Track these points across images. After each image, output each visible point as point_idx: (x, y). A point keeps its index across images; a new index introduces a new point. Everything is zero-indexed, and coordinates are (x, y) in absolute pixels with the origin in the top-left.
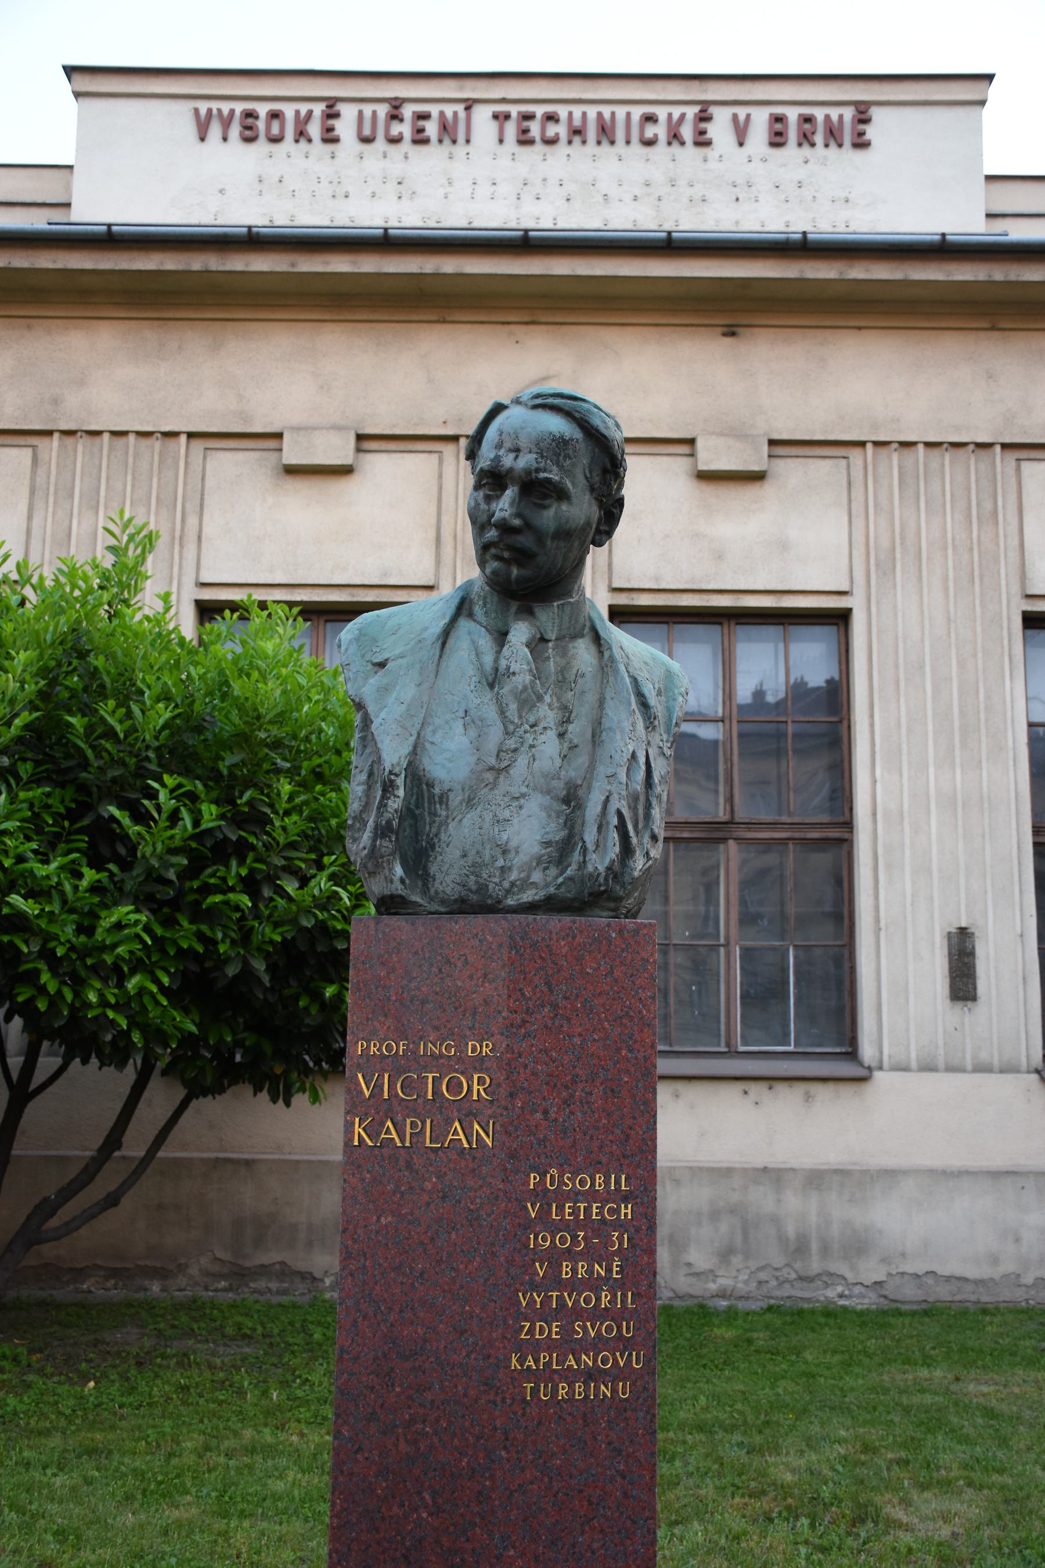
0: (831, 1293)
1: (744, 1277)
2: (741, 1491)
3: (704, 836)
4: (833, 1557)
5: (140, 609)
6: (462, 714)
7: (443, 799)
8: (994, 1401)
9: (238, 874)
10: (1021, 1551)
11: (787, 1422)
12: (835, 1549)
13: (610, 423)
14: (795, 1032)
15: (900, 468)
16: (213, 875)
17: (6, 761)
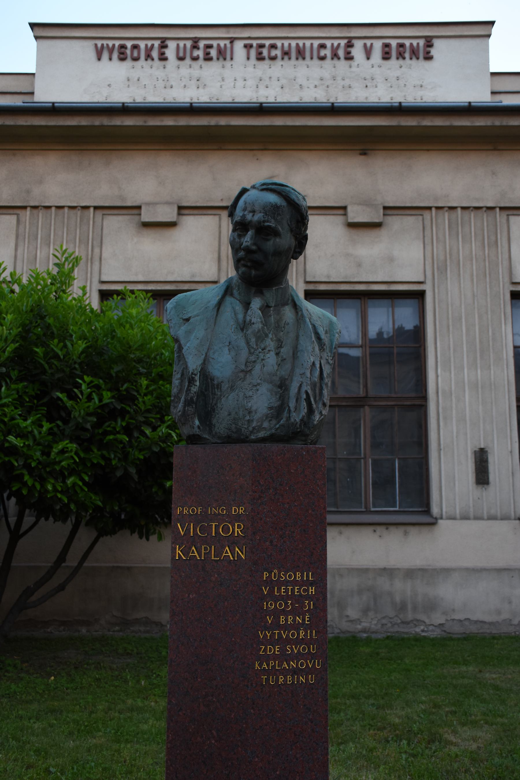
0: (418, 630)
1: (375, 622)
2: (373, 728)
4: (419, 759)
5: (71, 294)
6: (227, 344)
7: (219, 386)
8: (499, 682)
9: (121, 425)
10: (511, 755)
11: (396, 693)
12: (420, 755)
13: (300, 197)
14: (399, 501)
15: (449, 220)
16: (109, 426)
17: (4, 370)
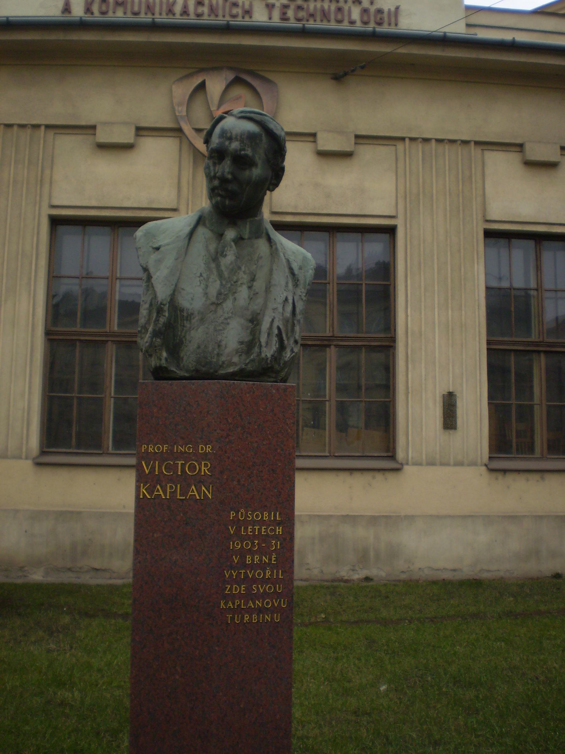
3: (317, 346)
15: (423, 152)
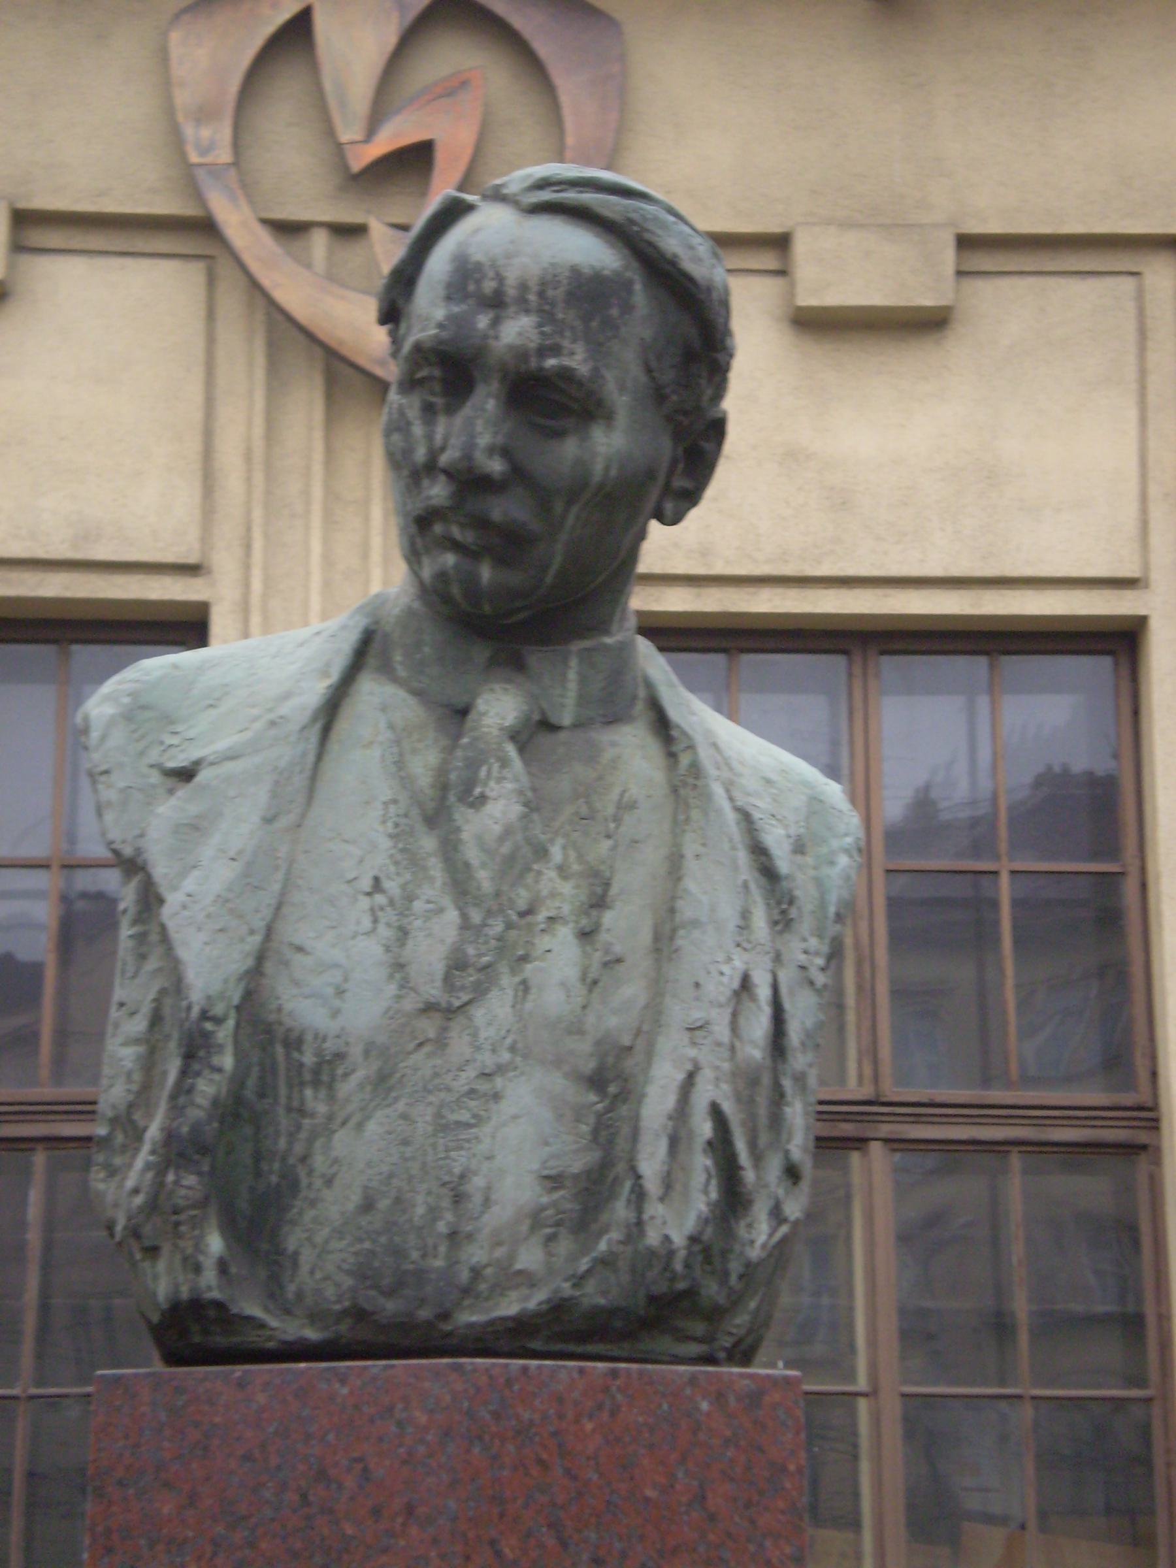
6: (366, 884)
